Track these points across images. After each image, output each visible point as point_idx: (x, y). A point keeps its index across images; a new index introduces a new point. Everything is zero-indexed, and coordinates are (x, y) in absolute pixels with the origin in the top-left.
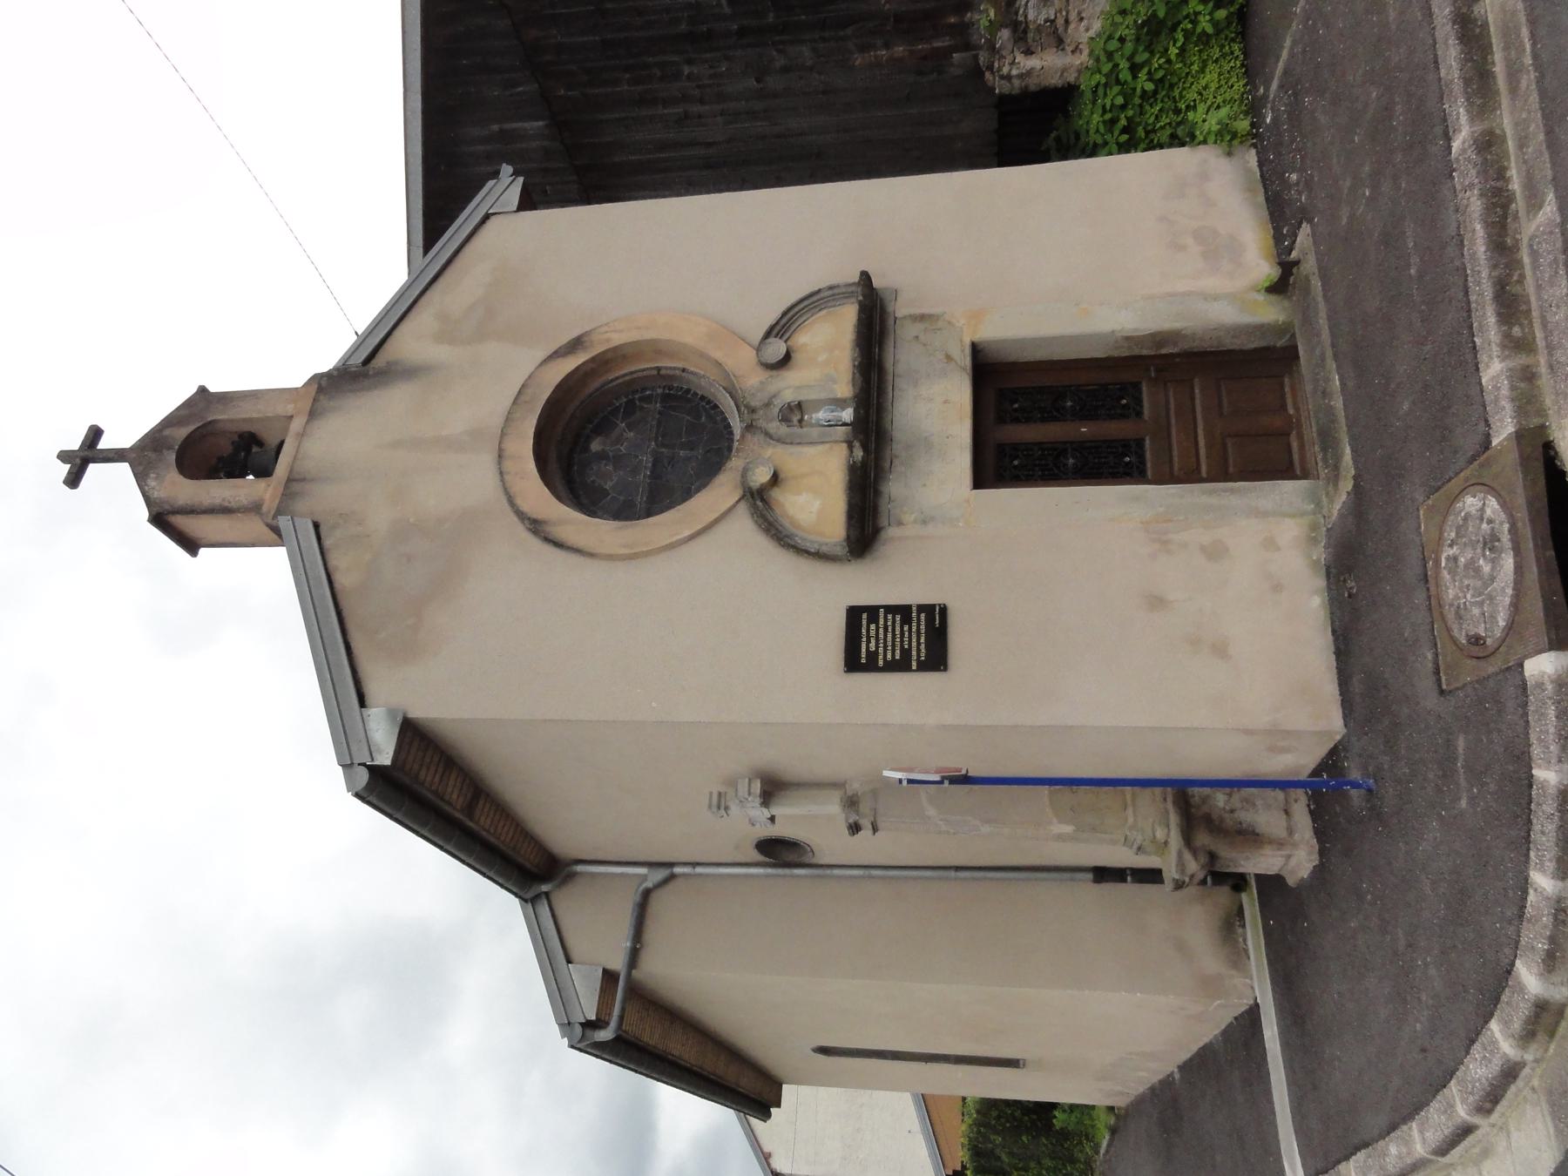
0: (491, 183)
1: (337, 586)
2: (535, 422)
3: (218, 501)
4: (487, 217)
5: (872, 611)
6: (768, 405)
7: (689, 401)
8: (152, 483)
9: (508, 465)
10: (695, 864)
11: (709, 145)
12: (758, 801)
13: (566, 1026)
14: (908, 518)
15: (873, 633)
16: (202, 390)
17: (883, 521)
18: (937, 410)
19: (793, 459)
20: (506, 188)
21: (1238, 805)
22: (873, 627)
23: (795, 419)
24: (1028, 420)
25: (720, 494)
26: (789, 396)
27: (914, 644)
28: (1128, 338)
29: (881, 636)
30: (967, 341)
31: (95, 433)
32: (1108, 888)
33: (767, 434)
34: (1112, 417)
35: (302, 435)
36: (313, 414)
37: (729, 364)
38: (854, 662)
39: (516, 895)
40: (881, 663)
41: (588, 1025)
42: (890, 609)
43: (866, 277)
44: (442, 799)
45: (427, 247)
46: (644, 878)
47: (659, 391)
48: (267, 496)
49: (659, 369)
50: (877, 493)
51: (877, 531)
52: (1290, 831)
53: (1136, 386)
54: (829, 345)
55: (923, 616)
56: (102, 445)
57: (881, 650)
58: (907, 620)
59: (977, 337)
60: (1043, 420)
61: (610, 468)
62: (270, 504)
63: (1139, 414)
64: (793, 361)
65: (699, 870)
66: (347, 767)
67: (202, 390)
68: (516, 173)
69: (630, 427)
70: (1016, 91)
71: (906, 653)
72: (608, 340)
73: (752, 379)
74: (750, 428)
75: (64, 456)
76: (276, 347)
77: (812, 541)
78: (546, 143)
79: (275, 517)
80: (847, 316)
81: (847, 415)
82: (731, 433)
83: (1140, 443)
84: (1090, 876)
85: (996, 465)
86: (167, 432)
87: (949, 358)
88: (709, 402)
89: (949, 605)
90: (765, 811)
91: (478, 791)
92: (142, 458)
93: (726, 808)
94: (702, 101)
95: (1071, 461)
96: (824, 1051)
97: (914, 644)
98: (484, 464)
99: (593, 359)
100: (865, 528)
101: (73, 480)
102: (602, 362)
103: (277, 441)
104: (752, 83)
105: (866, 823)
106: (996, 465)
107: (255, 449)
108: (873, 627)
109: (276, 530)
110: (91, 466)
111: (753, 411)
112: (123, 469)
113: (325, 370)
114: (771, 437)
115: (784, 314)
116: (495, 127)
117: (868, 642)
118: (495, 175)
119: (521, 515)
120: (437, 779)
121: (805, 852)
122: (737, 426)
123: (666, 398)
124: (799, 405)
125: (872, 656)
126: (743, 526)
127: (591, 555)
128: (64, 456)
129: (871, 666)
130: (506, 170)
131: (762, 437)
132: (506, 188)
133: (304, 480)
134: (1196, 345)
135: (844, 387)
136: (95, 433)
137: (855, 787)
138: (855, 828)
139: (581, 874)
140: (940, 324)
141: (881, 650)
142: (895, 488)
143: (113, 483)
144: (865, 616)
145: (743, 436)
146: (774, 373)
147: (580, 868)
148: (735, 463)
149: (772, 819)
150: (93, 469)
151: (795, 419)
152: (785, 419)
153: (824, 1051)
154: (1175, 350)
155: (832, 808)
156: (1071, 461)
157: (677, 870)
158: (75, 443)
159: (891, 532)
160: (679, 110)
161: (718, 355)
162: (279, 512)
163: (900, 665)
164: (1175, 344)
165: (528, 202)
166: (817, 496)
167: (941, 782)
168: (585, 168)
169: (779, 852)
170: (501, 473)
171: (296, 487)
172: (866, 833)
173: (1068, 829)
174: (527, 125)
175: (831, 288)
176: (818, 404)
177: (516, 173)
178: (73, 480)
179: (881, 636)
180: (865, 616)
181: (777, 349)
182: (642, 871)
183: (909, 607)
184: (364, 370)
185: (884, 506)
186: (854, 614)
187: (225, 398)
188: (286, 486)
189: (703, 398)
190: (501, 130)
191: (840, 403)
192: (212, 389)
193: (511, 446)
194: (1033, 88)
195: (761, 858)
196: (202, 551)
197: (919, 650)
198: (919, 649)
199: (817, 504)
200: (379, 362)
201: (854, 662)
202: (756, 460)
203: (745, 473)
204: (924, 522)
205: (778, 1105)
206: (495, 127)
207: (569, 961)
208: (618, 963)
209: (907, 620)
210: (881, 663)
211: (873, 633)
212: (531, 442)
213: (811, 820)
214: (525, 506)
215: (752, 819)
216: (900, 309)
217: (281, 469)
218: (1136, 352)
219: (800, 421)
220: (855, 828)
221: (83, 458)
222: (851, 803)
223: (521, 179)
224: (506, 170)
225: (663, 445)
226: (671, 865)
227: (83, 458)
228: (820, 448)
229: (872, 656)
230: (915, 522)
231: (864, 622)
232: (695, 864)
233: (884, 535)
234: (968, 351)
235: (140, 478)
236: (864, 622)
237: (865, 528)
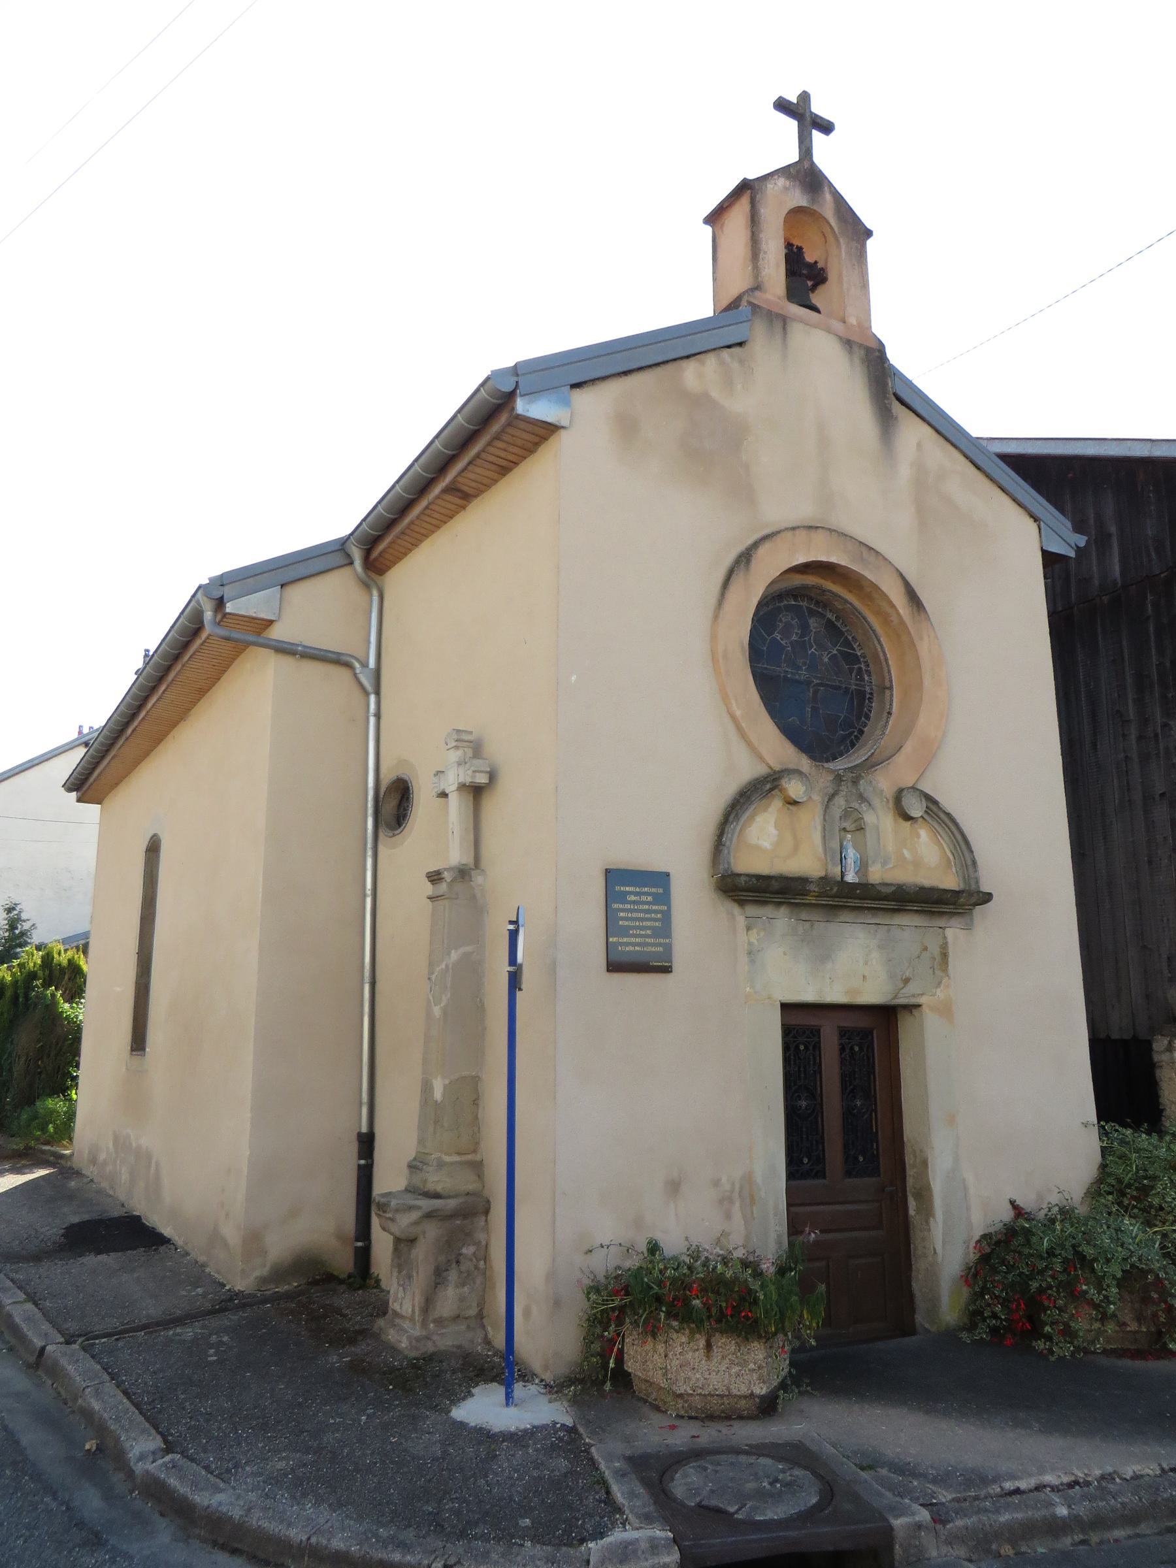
0: (1069, 525)
1: (684, 363)
2: (843, 563)
3: (764, 246)
4: (1036, 519)
5: (664, 898)
6: (862, 798)
7: (859, 718)
8: (781, 182)
9: (802, 534)
10: (378, 716)
11: (1094, 745)
12: (468, 780)
13: (222, 581)
14: (754, 937)
15: (644, 898)
16: (869, 233)
17: (752, 910)
18: (853, 967)
19: (811, 822)
20: (1068, 541)
21: (463, 1268)
22: (650, 898)
23: (848, 825)
24: (842, 1062)
25: (776, 749)
26: (869, 818)
27: (633, 940)
28: (925, 1163)
29: (641, 907)
30: (922, 1000)
31: (826, 128)
32: (353, 1148)
33: (832, 797)
34: (846, 1146)
35: (829, 331)
36: (848, 344)
37: (899, 758)
38: (617, 880)
39: (352, 534)
40: (615, 906)
41: (220, 603)
42: (667, 917)
43: (987, 898)
44: (470, 463)
45: (1006, 458)
46: (365, 665)
47: (867, 689)
48: (768, 296)
49: (891, 688)
50: (779, 904)
51: (741, 903)
52: (439, 1322)
53: (875, 1172)
54: (919, 859)
55: (661, 949)
56: (816, 134)
57: (628, 906)
58: (656, 933)
59: (925, 1009)
60: (843, 1076)
61: (794, 638)
62: (759, 298)
63: (849, 1174)
64: (901, 821)
65: (372, 720)
66: (515, 370)
67: (869, 233)
68: (1078, 549)
69: (833, 658)
70: (1156, 1058)
71: (624, 931)
72: (921, 638)
73: (884, 782)
74: (839, 778)
75: (805, 97)
76: (909, 305)
77: (731, 839)
78: (1096, 582)
79: (750, 303)
80: (950, 881)
81: (850, 878)
82: (828, 761)
83: (821, 1174)
84: (364, 1130)
85: (802, 1027)
86: (828, 197)
87: (907, 981)
88: (857, 738)
89: (670, 975)
90: (455, 787)
91: (463, 496)
92: (806, 175)
93: (457, 747)
94: (1140, 738)
95: (804, 1104)
96: (153, 849)
97: (633, 940)
98: (803, 510)
99: (902, 622)
100: (747, 891)
101: (782, 106)
102: (900, 631)
103: (818, 305)
104: (1160, 788)
105: (443, 887)
106: (802, 1027)
107: (810, 283)
108: (650, 898)
109: (734, 305)
110: (796, 123)
111: (855, 782)
112: (791, 155)
113: (888, 356)
114: (830, 800)
115: (948, 815)
116: (1113, 529)
117: (636, 894)
118: (1079, 528)
119: (756, 545)
120: (492, 458)
121: (392, 828)
122: (840, 765)
123: (861, 695)
124: (861, 829)
125: (622, 897)
126: (748, 770)
127: (716, 617)
128: (805, 97)
129: (610, 896)
130: (1082, 540)
131: (831, 791)
132: (1068, 541)
133: (784, 328)
134: (916, 1236)
135: (876, 874)
136: (826, 128)
137: (479, 879)
138: (435, 877)
139: (371, 595)
140: (938, 973)
141: (628, 906)
142: (781, 919)
143: (779, 145)
144: (661, 891)
145: (832, 771)
146: (891, 805)
147: (376, 598)
148: (804, 763)
149: (444, 795)
150: (792, 125)
151: (848, 825)
152: (846, 815)
153: (153, 849)
154: (912, 1212)
155: (456, 854)
156: (804, 1104)
157: (373, 698)
158: (818, 107)
159: (739, 916)
160: (1131, 713)
161: (908, 748)
162: (755, 308)
163: (611, 925)
164: (918, 1211)
165: (1050, 560)
166: (775, 843)
167: (513, 960)
168: (1079, 616)
169: (395, 804)
170: (794, 529)
171: (778, 325)
172: (429, 889)
173: (438, 1094)
174: (1116, 559)
175: (974, 863)
176: (860, 848)
177: (1078, 549)
178: (782, 106)
179: (641, 907)
180: (661, 891)
181: (916, 808)
182: (372, 663)
183: (669, 936)
184: (890, 393)
185: (767, 911)
186: (661, 879)
187: (860, 256)
188: (778, 316)
189: (861, 732)
190: (1110, 535)
191: (863, 867)
192: (870, 243)
193: (819, 537)
194: (1158, 1073)
195: (386, 780)
196: (708, 229)
197: (627, 944)
198: (630, 946)
199: (766, 844)
200: (897, 407)
201: (617, 880)
202: (807, 783)
203: (798, 772)
204: (749, 953)
205: (79, 800)
206: (1113, 529)
207: (282, 586)
208: (277, 633)
209: (656, 933)
210: (615, 906)
211: (644, 898)
212: (824, 559)
213: (436, 836)
214: (762, 551)
215: (437, 772)
216: (954, 932)
217: (795, 310)
218: (910, 1172)
219: (844, 829)
220: (435, 877)
221: (803, 115)
222: (463, 873)
223: (1072, 554)
224: (1082, 540)
225: (816, 692)
226: (378, 693)
227: (803, 115)
228: (820, 849)
229: (622, 897)
230: (750, 944)
231: (654, 890)
232: (378, 716)
233: (736, 909)
234: (913, 1001)
235: (785, 171)
236: (654, 890)
237: (747, 891)
